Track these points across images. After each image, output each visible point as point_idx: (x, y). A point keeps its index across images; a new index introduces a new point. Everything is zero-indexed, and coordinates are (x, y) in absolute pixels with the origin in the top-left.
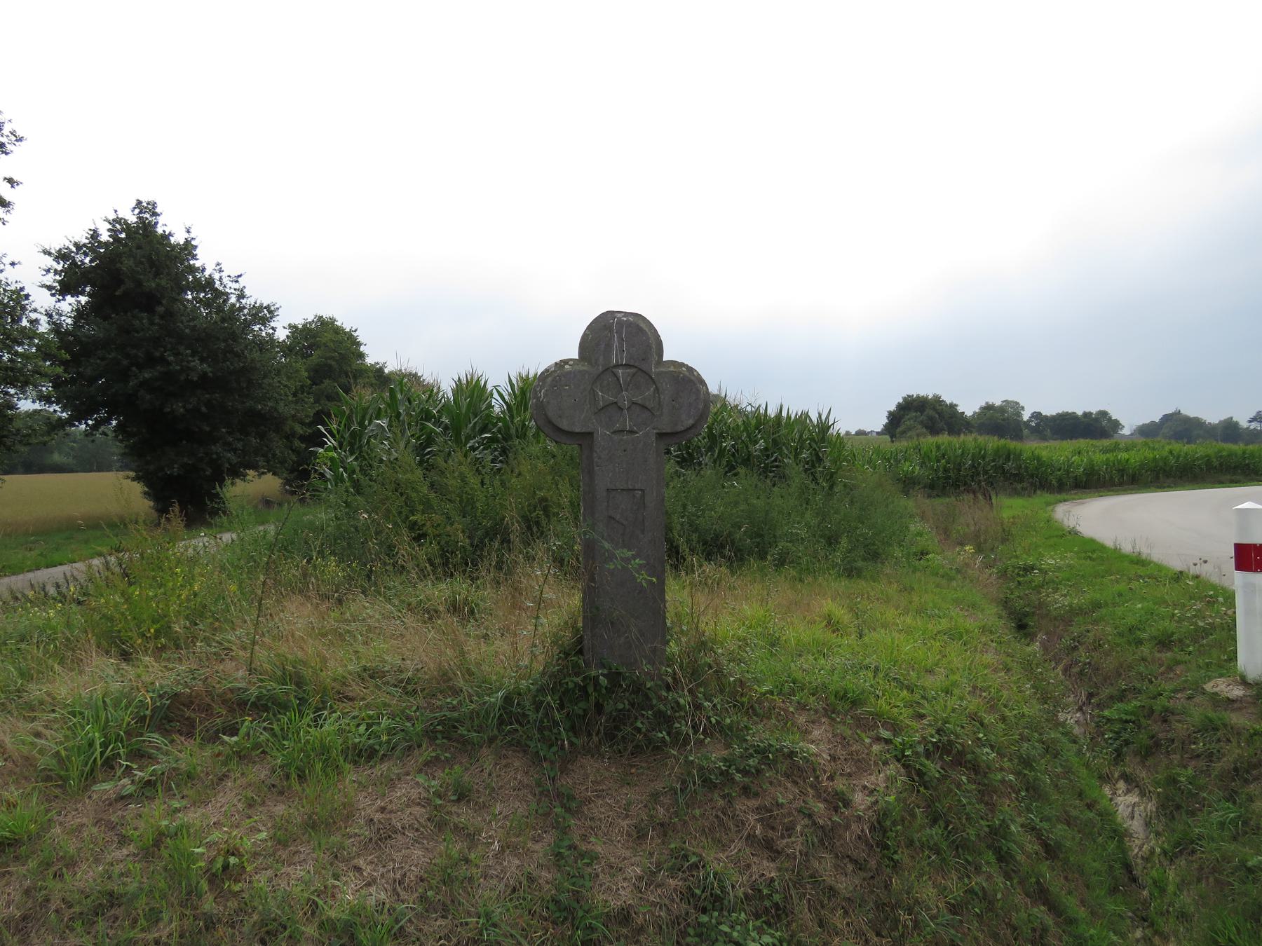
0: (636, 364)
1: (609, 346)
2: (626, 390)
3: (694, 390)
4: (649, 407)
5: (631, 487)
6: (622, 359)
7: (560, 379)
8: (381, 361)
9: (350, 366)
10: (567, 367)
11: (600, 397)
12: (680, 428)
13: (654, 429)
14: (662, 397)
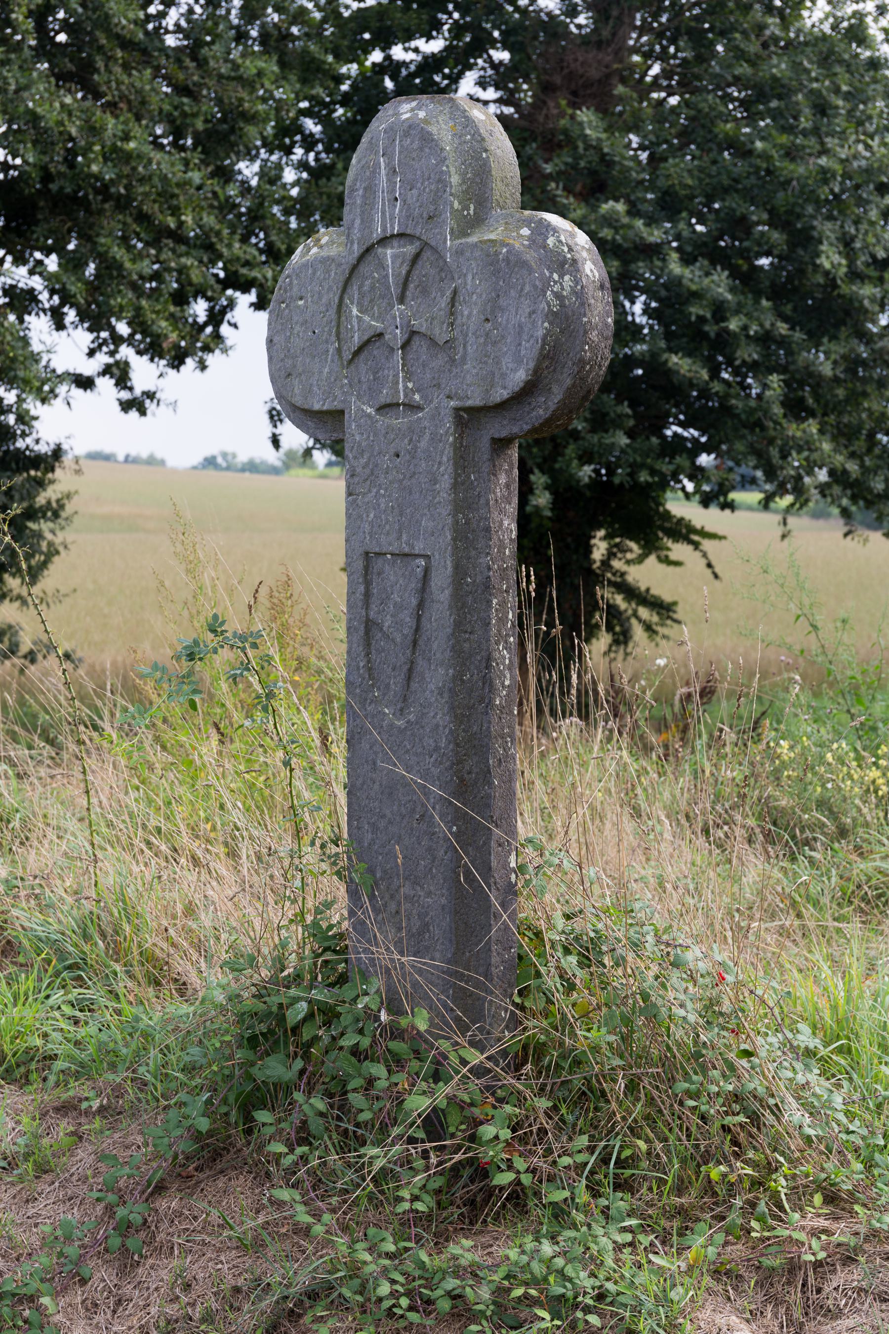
3: (527, 288)
5: (407, 550)
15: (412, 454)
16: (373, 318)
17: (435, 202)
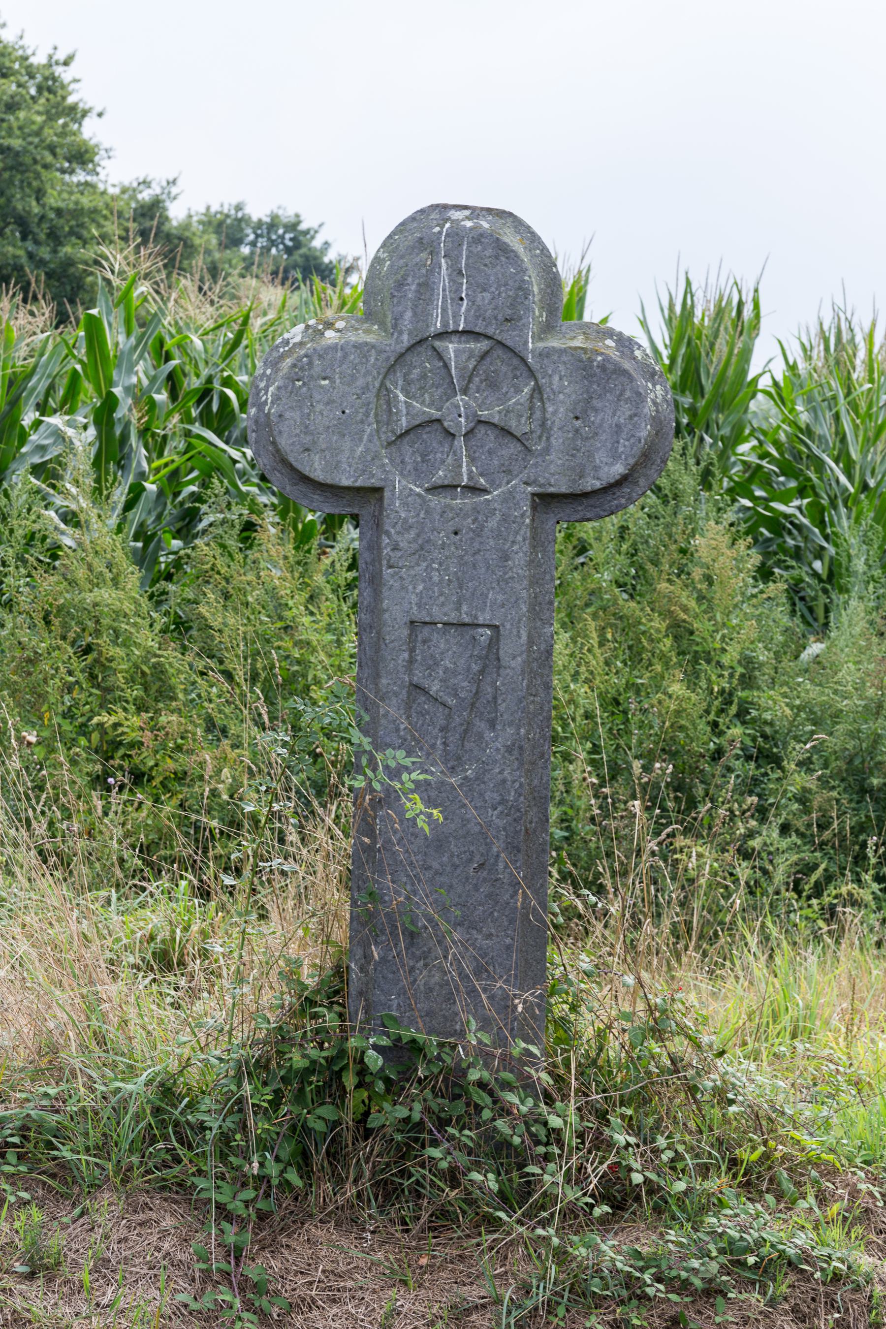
0: (490, 331)
1: (426, 287)
2: (465, 392)
3: (628, 394)
4: (518, 434)
5: (467, 620)
6: (456, 316)
7: (310, 363)
8: (159, 175)
9: (40, 194)
10: (330, 334)
11: (402, 407)
12: (591, 483)
13: (527, 483)
14: (550, 409)
15: (478, 532)
16: (423, 403)
17: (512, 306)
